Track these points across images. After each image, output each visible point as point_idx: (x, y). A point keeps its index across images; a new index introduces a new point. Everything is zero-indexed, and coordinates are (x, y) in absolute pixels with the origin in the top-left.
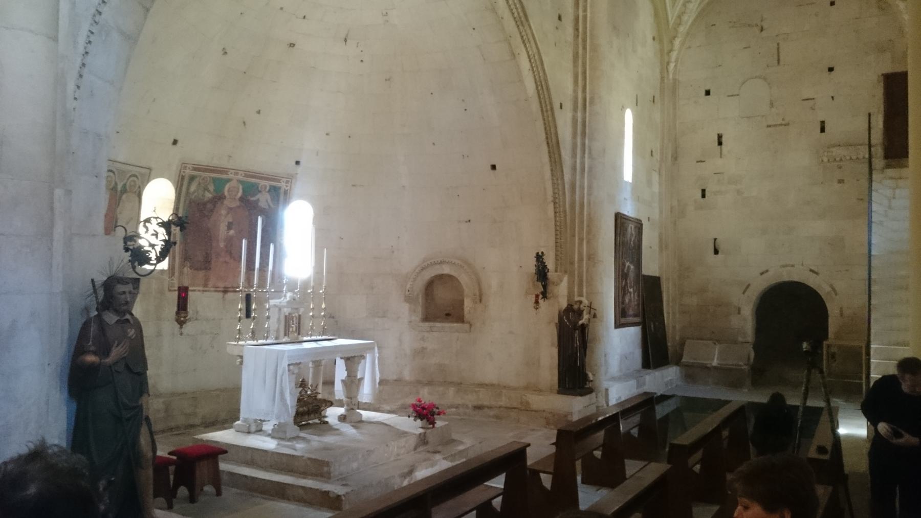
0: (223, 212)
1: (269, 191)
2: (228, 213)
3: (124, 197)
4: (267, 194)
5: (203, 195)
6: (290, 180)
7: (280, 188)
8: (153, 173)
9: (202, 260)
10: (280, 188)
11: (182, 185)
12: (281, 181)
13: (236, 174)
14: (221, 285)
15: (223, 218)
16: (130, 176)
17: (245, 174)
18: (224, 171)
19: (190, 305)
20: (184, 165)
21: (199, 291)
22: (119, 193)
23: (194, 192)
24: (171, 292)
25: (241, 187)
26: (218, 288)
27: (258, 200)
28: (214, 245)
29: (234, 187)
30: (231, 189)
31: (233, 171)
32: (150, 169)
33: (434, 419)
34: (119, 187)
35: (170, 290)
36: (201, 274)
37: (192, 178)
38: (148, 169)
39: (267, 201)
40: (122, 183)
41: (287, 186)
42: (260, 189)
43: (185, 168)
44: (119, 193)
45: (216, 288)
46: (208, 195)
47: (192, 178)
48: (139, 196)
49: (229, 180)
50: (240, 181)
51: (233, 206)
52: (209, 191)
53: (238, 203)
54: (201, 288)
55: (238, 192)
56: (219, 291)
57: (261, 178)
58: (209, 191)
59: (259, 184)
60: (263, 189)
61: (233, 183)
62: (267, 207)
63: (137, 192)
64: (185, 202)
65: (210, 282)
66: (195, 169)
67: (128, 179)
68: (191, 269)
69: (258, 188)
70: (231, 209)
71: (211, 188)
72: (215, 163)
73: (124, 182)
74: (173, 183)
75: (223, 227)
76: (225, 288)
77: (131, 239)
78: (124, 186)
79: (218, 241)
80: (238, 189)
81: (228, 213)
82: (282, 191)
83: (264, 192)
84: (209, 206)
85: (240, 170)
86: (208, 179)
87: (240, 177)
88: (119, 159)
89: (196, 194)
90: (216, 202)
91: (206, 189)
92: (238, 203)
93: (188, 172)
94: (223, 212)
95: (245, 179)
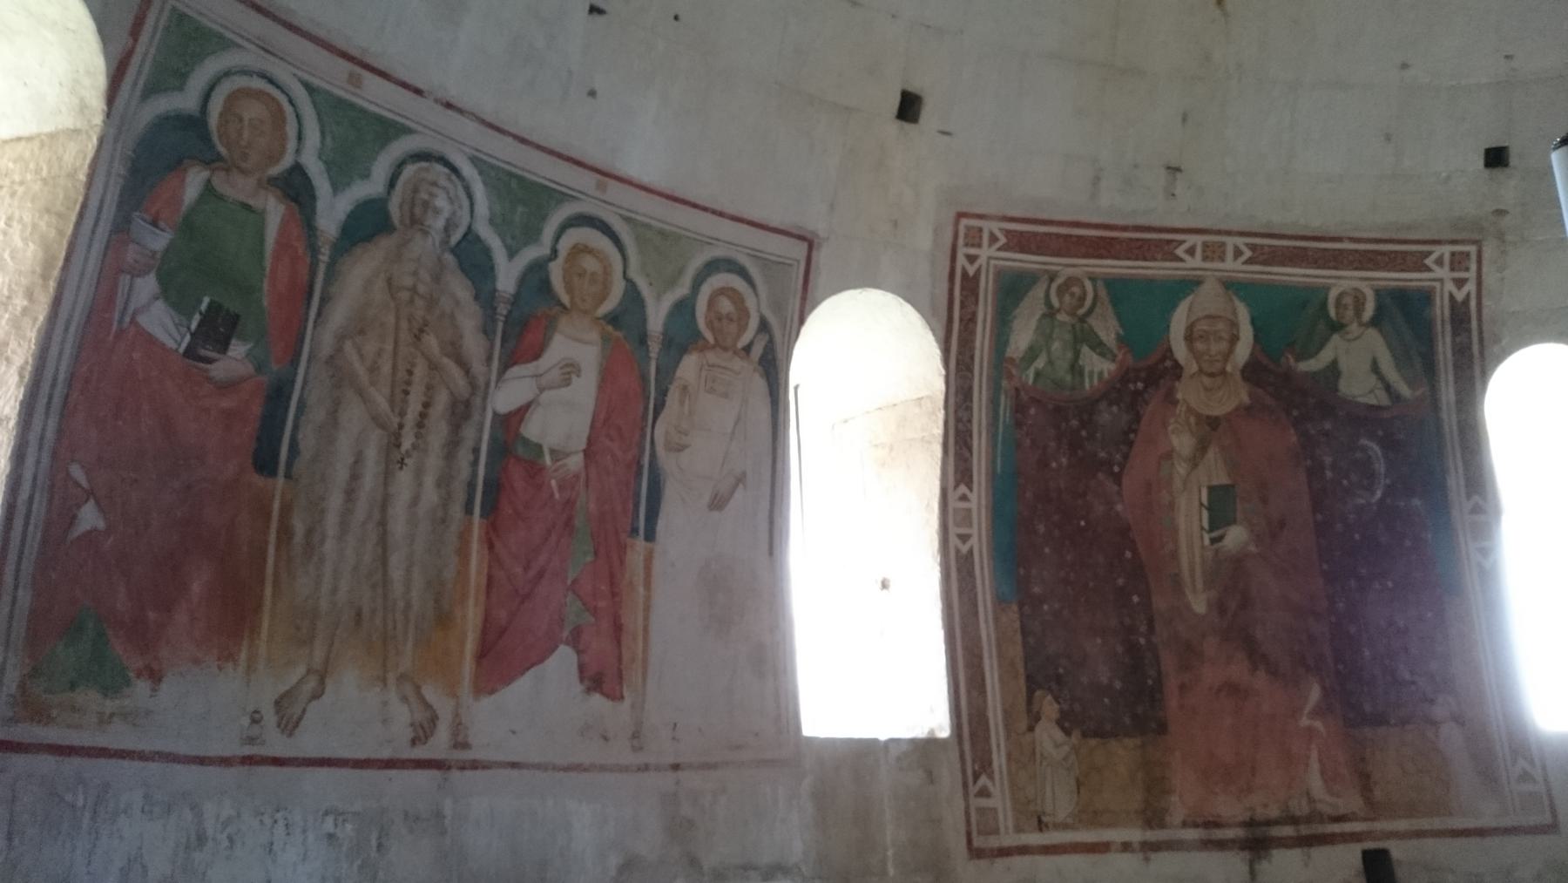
0: (1183, 442)
1: (1375, 322)
3: (689, 367)
4: (1373, 335)
5: (1076, 369)
6: (1472, 249)
7: (1426, 297)
8: (822, 257)
9: (1118, 685)
10: (1426, 297)
11: (969, 321)
12: (1429, 261)
13: (1213, 252)
14: (1230, 808)
15: (1181, 469)
16: (712, 267)
17: (1253, 247)
20: (964, 222)
21: (1126, 847)
22: (654, 348)
23: (1032, 354)
24: (983, 863)
25: (1243, 314)
26: (1217, 825)
27: (1333, 370)
28: (1160, 603)
29: (1211, 317)
30: (1203, 326)
31: (962, 251)
32: (810, 242)
34: (656, 317)
35: (976, 853)
36: (1123, 754)
37: (1013, 289)
38: (801, 238)
39: (1375, 368)
40: (669, 299)
41: (1460, 283)
42: (1332, 312)
43: (974, 238)
45: (1208, 825)
46: (1098, 367)
47: (1013, 289)
48: (773, 369)
49: (1189, 285)
50: (1231, 286)
51: (1218, 410)
53: (1242, 394)
54: (1135, 835)
55: (1234, 339)
56: (1221, 845)
57: (1336, 260)
58: (1098, 346)
59: (1327, 289)
60: (1350, 313)
61: (1209, 299)
62: (1382, 398)
63: (757, 351)
64: (994, 403)
65: (1174, 798)
66: (1020, 243)
68: (1067, 732)
69: (1324, 305)
70: (1213, 423)
71: (1107, 329)
73: (683, 290)
74: (928, 314)
76: (1250, 824)
77: (453, 344)
78: (684, 308)
79: (1177, 584)
80: (1234, 325)
81: (1202, 447)
82: (1441, 310)
83: (1354, 328)
84: (1106, 416)
85: (1229, 233)
86: (1089, 285)
87: (1231, 266)
88: (632, 170)
89: (1040, 363)
90: (1137, 393)
91: (1083, 336)
92: (1242, 394)
93: (990, 258)
95: (1258, 272)
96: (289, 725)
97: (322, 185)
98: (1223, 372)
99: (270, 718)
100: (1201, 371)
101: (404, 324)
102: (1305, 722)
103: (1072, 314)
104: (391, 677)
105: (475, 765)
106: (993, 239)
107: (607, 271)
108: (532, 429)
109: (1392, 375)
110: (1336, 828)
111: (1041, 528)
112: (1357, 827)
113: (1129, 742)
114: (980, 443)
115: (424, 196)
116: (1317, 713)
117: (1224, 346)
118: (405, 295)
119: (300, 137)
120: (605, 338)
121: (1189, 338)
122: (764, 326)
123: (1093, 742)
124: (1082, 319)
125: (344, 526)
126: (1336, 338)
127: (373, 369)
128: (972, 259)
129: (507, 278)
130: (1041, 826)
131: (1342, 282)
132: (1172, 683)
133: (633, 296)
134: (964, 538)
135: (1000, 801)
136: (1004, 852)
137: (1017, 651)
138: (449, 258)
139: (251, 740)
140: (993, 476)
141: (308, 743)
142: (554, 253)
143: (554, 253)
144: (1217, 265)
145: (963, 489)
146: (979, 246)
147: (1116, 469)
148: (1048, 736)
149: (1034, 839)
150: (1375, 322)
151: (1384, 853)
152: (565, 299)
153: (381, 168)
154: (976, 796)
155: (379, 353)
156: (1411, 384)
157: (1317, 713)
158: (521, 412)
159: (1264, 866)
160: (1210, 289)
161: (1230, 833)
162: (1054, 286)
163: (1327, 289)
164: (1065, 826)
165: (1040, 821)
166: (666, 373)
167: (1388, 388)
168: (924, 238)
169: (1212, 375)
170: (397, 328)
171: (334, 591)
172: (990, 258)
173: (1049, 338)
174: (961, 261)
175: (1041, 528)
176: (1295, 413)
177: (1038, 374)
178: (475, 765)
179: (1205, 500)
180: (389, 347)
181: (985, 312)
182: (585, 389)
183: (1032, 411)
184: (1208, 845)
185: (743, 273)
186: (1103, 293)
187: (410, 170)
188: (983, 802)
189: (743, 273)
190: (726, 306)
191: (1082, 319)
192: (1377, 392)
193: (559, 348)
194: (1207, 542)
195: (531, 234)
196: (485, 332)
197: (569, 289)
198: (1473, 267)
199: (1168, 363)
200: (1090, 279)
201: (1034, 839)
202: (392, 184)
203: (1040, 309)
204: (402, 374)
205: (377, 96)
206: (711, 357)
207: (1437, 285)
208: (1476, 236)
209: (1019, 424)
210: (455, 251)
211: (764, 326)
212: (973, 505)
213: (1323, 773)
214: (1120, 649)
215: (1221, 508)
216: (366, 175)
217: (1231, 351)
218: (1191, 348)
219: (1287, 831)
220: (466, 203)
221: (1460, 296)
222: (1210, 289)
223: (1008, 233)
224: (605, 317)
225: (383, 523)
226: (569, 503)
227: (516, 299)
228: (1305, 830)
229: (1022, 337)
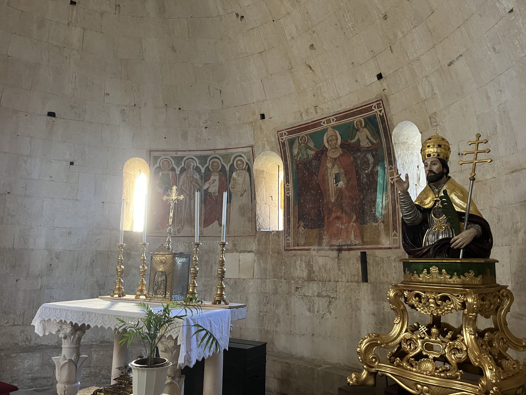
1: (365, 126)
2: (333, 166)
3: (234, 175)
4: (365, 129)
8: (255, 149)
10: (375, 116)
11: (285, 152)
13: (329, 121)
14: (337, 242)
16: (236, 157)
18: (316, 124)
19: (369, 276)
20: (279, 133)
22: (228, 173)
23: (298, 154)
31: (325, 120)
33: (168, 352)
34: (227, 168)
35: (286, 250)
36: (315, 231)
39: (367, 138)
43: (282, 135)
44: (228, 173)
46: (312, 153)
47: (291, 142)
49: (326, 130)
50: (334, 128)
52: (310, 149)
53: (340, 151)
54: (316, 247)
55: (337, 139)
56: (333, 250)
57: (353, 114)
58: (310, 149)
60: (359, 126)
61: (330, 132)
64: (292, 165)
66: (290, 133)
67: (233, 161)
68: (305, 228)
70: (335, 159)
71: (311, 145)
72: (306, 119)
75: (331, 181)
78: (232, 165)
80: (336, 136)
81: (333, 166)
82: (379, 120)
84: (314, 163)
86: (306, 137)
87: (333, 123)
94: (329, 165)
96: (179, 233)
97: (176, 168)
98: (336, 147)
99: (177, 232)
100: (331, 148)
101: (189, 182)
102: (352, 224)
103: (304, 143)
104: (192, 226)
105: (204, 236)
106: (285, 134)
107: (218, 164)
108: (210, 190)
109: (371, 139)
110: (356, 247)
111: (303, 189)
112: (360, 247)
113: (316, 230)
114: (290, 175)
115: (189, 164)
116: (355, 222)
117: (335, 141)
118: (189, 178)
119: (172, 163)
120: (219, 174)
121: (328, 142)
122: (247, 164)
123: (309, 230)
124: (306, 144)
125: (185, 208)
126: (358, 133)
127: (186, 188)
128: (282, 139)
129: (203, 170)
130: (298, 245)
131: (356, 119)
132: (326, 218)
133: (223, 166)
134: (288, 193)
135: (291, 241)
136: (291, 250)
137: (297, 214)
138: (195, 171)
139: (174, 234)
140: (293, 180)
141: (181, 235)
142: (209, 164)
143: (209, 164)
144: (330, 124)
145: (288, 184)
146: (283, 136)
147: (317, 174)
148: (301, 229)
149: (297, 248)
150: (365, 126)
151: (365, 252)
152: (212, 170)
153: (183, 163)
154: (393, 236)
155: (187, 186)
156: (376, 140)
157: (355, 222)
158: (208, 188)
159: (340, 254)
160: (330, 130)
161: (334, 248)
162: (299, 139)
163: (353, 122)
164: (302, 246)
165: (298, 245)
166: (230, 177)
167: (370, 141)
168: (273, 139)
169: (334, 149)
170: (188, 182)
171: (184, 217)
172: (285, 138)
173: (301, 150)
174: (280, 140)
175: (303, 189)
176: (352, 153)
177: (300, 158)
178: (204, 236)
179: (334, 178)
180: (188, 185)
181: (287, 148)
182: (217, 183)
183: (300, 165)
184: (330, 249)
185: (241, 156)
186: (309, 137)
187: (186, 162)
188: (288, 241)
189: (241, 156)
190: (239, 162)
191: (306, 144)
192: (369, 143)
193: (212, 178)
194: (335, 186)
195: (206, 163)
196: (201, 179)
197: (212, 169)
198: (382, 107)
199: (325, 149)
200: (306, 135)
201: (297, 248)
202: (185, 164)
203: (298, 144)
204: (190, 188)
205: (180, 154)
206: (238, 172)
207: (376, 113)
208: (381, 98)
209: (297, 169)
210: (195, 169)
211: (247, 164)
212: (290, 187)
213: (354, 235)
214: (316, 211)
215: (337, 179)
216: (181, 164)
217: (337, 142)
218: (329, 144)
219: (346, 247)
220: (195, 162)
221: (381, 114)
222: (330, 130)
223: (287, 132)
224: (219, 171)
225: (190, 207)
226: (216, 200)
227: (205, 173)
228: (349, 247)
229: (295, 151)
